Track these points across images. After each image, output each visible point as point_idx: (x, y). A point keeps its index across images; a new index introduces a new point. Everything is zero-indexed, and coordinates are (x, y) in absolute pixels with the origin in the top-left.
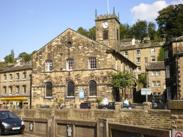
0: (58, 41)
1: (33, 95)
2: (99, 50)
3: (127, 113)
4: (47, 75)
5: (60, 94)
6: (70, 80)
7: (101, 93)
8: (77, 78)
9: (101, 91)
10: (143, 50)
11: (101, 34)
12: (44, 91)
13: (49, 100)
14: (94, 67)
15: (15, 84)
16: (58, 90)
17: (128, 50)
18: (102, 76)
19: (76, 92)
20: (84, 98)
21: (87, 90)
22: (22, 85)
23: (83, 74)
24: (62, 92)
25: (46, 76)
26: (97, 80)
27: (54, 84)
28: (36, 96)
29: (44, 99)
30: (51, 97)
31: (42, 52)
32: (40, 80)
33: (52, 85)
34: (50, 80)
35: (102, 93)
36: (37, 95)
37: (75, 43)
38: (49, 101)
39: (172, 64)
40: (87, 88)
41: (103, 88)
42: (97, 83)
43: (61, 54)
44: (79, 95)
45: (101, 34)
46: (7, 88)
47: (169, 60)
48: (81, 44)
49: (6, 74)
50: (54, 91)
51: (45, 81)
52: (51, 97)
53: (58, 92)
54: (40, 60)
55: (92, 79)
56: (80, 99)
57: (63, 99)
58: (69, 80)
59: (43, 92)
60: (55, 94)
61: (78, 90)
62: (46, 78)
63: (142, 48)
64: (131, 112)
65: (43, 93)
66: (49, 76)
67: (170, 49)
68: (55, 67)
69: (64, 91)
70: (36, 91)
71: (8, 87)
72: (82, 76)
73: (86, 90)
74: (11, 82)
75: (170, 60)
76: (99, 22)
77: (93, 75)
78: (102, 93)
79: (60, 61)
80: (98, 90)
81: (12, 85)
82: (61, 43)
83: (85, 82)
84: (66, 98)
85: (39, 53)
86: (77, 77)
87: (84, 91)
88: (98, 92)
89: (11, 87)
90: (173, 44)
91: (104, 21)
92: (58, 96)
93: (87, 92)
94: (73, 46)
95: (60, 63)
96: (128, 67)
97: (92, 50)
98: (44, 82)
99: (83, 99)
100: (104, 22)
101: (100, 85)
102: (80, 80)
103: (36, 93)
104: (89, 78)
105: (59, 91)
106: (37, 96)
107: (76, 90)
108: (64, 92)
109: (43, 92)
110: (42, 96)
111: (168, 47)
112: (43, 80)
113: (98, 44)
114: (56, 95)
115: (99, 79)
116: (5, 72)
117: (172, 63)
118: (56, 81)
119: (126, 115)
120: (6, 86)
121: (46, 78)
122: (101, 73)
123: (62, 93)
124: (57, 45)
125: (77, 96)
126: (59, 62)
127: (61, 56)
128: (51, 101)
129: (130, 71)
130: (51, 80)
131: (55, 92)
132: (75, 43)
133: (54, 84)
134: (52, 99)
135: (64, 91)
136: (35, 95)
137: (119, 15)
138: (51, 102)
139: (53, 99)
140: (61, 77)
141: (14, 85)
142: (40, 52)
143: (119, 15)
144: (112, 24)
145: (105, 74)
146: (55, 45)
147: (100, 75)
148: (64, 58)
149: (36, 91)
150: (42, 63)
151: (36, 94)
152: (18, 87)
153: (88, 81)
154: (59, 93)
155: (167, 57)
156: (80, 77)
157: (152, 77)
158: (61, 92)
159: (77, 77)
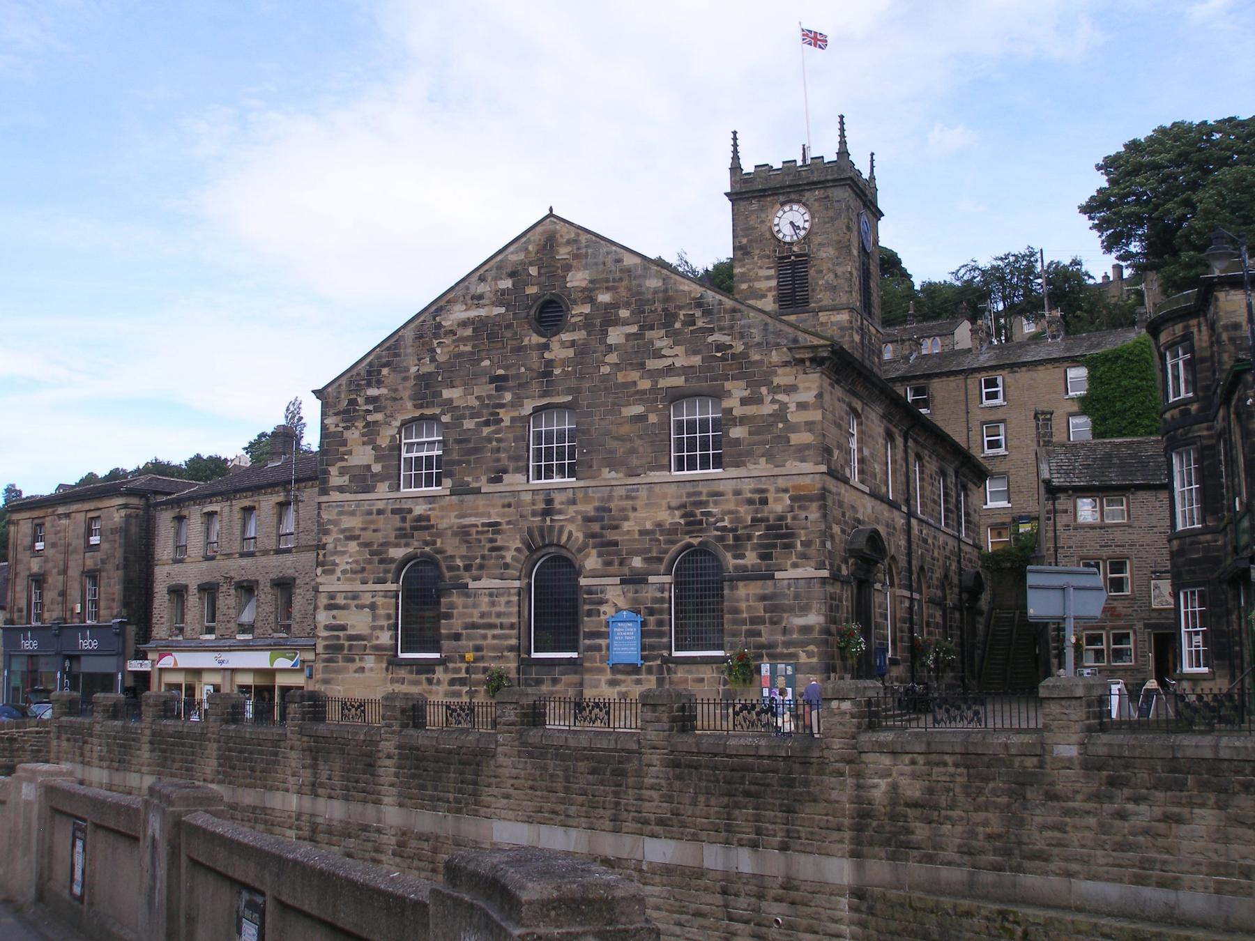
0: (481, 297)
1: (325, 638)
2: (739, 347)
3: (913, 762)
4: (410, 511)
5: (490, 633)
6: (551, 545)
7: (751, 634)
8: (594, 536)
9: (754, 621)
10: (1023, 376)
11: (768, 278)
12: (388, 617)
13: (418, 673)
14: (692, 460)
15: (232, 574)
16: (476, 612)
17: (929, 376)
18: (761, 520)
19: (588, 624)
20: (639, 662)
21: (661, 612)
22: (273, 576)
23: (634, 509)
24: (505, 620)
25: (404, 520)
26: (727, 548)
27: (450, 568)
28: (341, 647)
29: (394, 663)
30: (437, 655)
31: (385, 371)
32: (366, 545)
33: (440, 577)
34: (427, 543)
35: (759, 634)
36: (351, 638)
37: (586, 309)
38: (424, 677)
39: (1210, 437)
40: (662, 600)
41: (763, 598)
42: (730, 561)
43: (500, 382)
44: (608, 647)
45: (768, 278)
46: (193, 600)
47: (1194, 408)
48: (624, 313)
49: (185, 512)
50: (448, 616)
51: (397, 553)
52: (437, 655)
53: (474, 626)
54: (369, 418)
55: (695, 541)
56: (615, 669)
57: (510, 665)
58: (545, 546)
59: (385, 623)
60: (457, 637)
61: (603, 608)
62: (403, 536)
63: (1013, 367)
64: (948, 759)
65: (382, 628)
66: (420, 518)
67: (1196, 337)
68: (459, 463)
69: (514, 620)
70: (343, 618)
71: (193, 589)
72: (626, 519)
73: (651, 612)
74: (214, 563)
75: (1200, 410)
76: (755, 206)
77: (698, 512)
78: (759, 634)
79: (487, 423)
80: (736, 611)
81: (217, 577)
82: (503, 310)
83: (646, 560)
84: (526, 664)
85: (363, 373)
86: (596, 527)
87: (639, 619)
88: (734, 622)
89: (209, 590)
90: (1217, 299)
91: (782, 198)
92: (478, 648)
93: (660, 623)
94: (574, 328)
95: (489, 439)
96: (932, 466)
97: (695, 353)
98: (392, 560)
99: (633, 669)
100: (783, 204)
101: (747, 576)
102: (616, 544)
103: (343, 628)
104: (673, 530)
105: (483, 615)
106: (347, 644)
107: (589, 613)
108: (512, 626)
109: (385, 623)
110: (377, 648)
111: (1186, 328)
112: (386, 544)
113: (734, 311)
114: (464, 642)
115: (736, 538)
116: (179, 502)
117: (1209, 429)
118: (463, 550)
119: (903, 781)
120: (186, 587)
121: (403, 536)
122: (750, 502)
123: (502, 626)
124: (479, 325)
125: (598, 648)
126: (486, 431)
127: (498, 389)
128: (430, 681)
129: (946, 501)
130: (434, 543)
131: (456, 624)
132: (586, 309)
133: (450, 568)
134: (439, 669)
135: (514, 620)
136: (338, 638)
137: (872, 167)
138: (434, 688)
139: (446, 670)
140: (497, 524)
141: (229, 579)
142: (369, 373)
143: (872, 167)
144: (831, 213)
145: (779, 508)
146: (464, 324)
147: (746, 513)
148: (517, 403)
149: (343, 618)
150: (384, 442)
151: (341, 634)
152: (247, 589)
153: (666, 552)
154: (483, 632)
155: (1177, 393)
156: (616, 527)
157: (1079, 535)
158: (498, 621)
159: (596, 527)
